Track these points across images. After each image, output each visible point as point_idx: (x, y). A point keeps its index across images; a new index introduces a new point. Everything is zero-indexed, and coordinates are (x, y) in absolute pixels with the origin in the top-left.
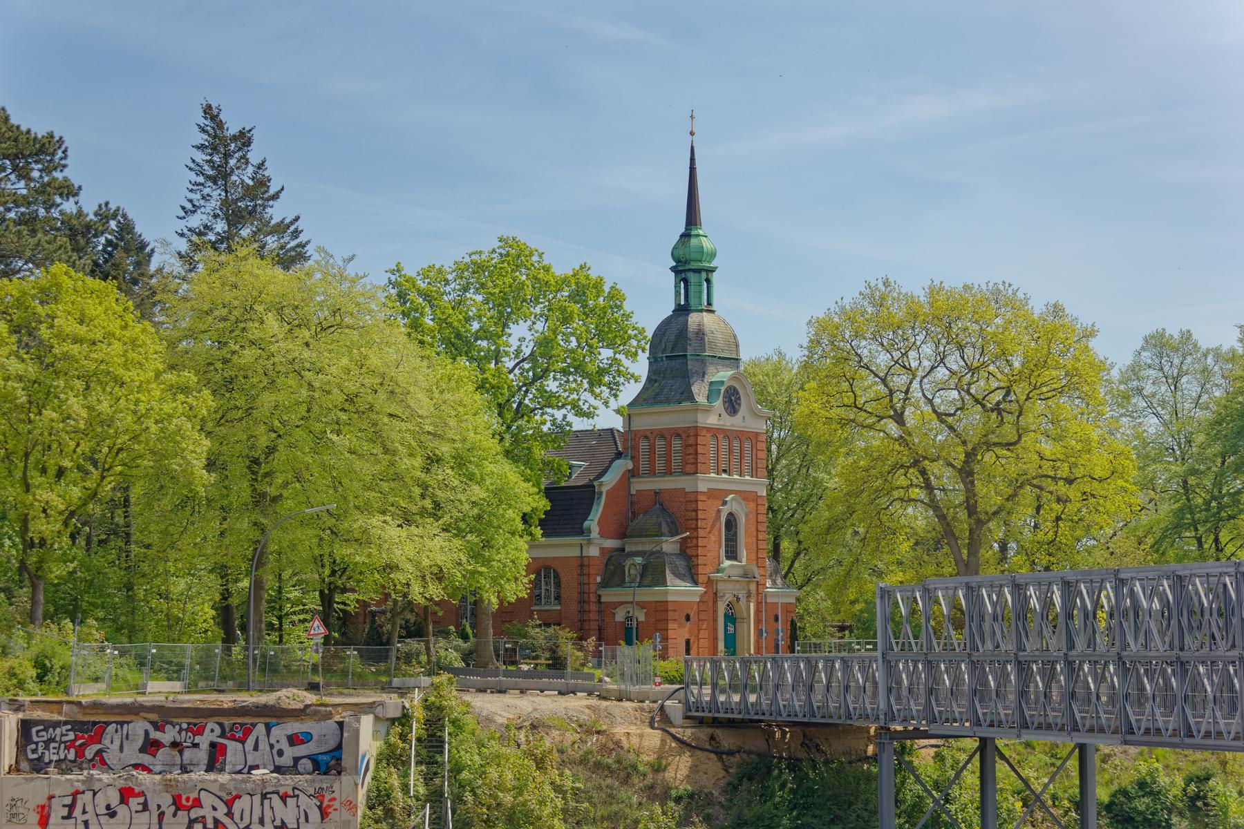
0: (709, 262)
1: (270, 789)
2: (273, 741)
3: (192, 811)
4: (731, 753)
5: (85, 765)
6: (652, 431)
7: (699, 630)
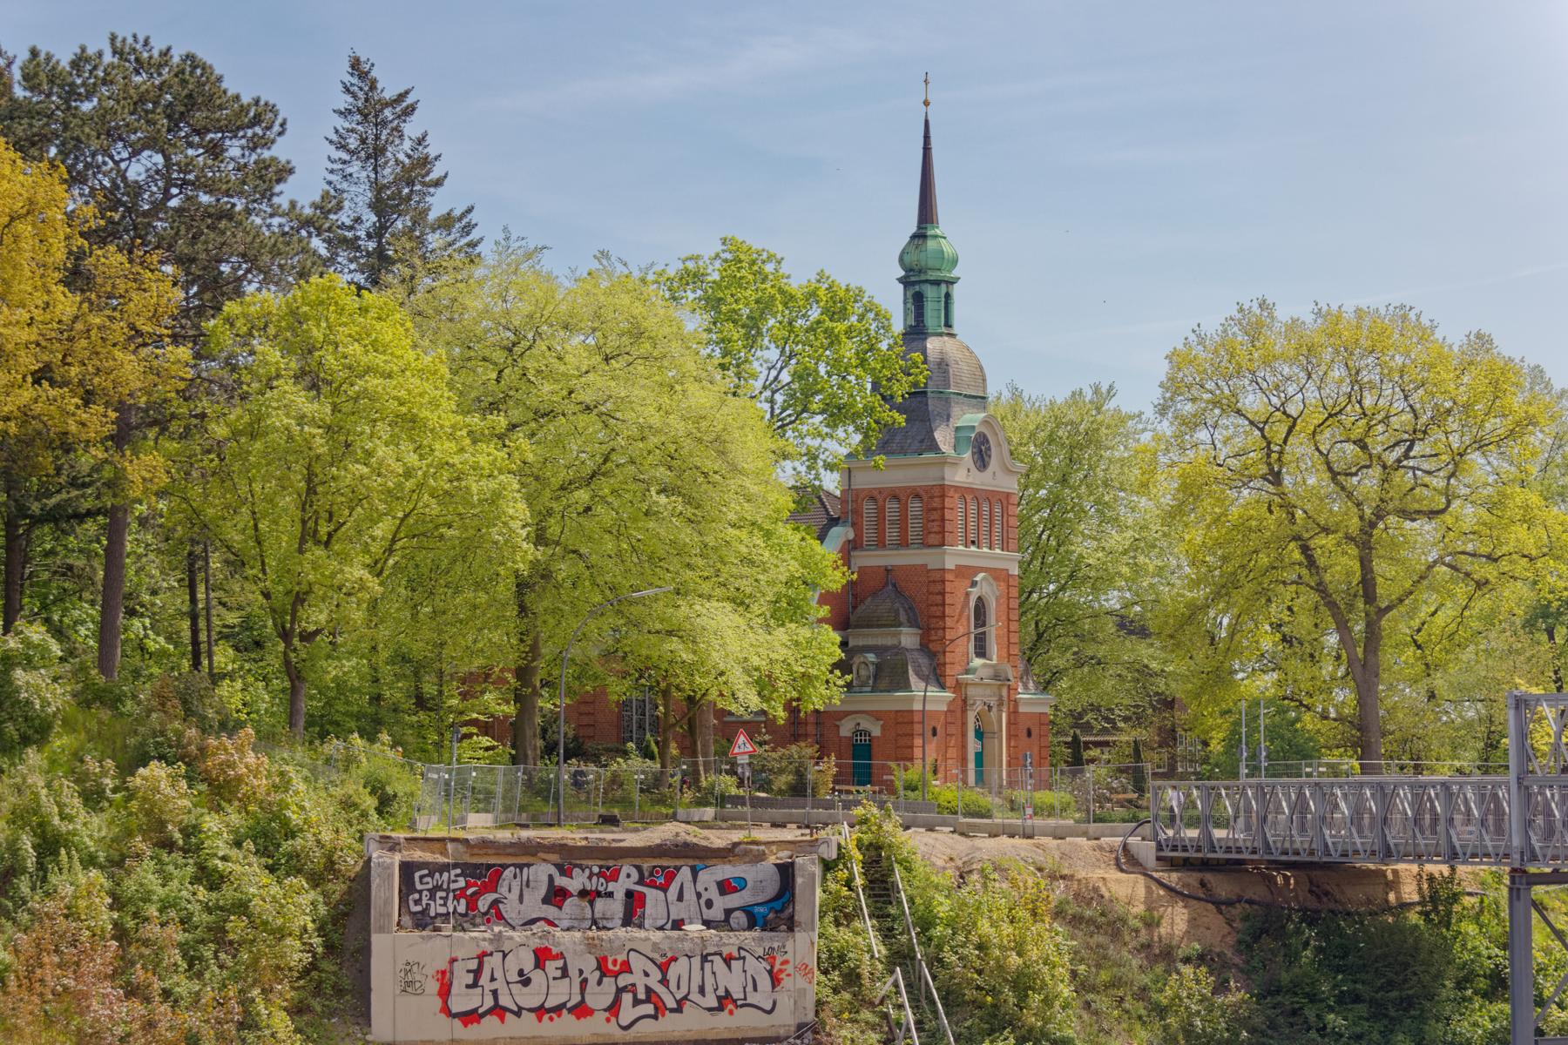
1: (711, 950)
2: (700, 888)
3: (621, 978)
5: (478, 920)
6: (880, 491)
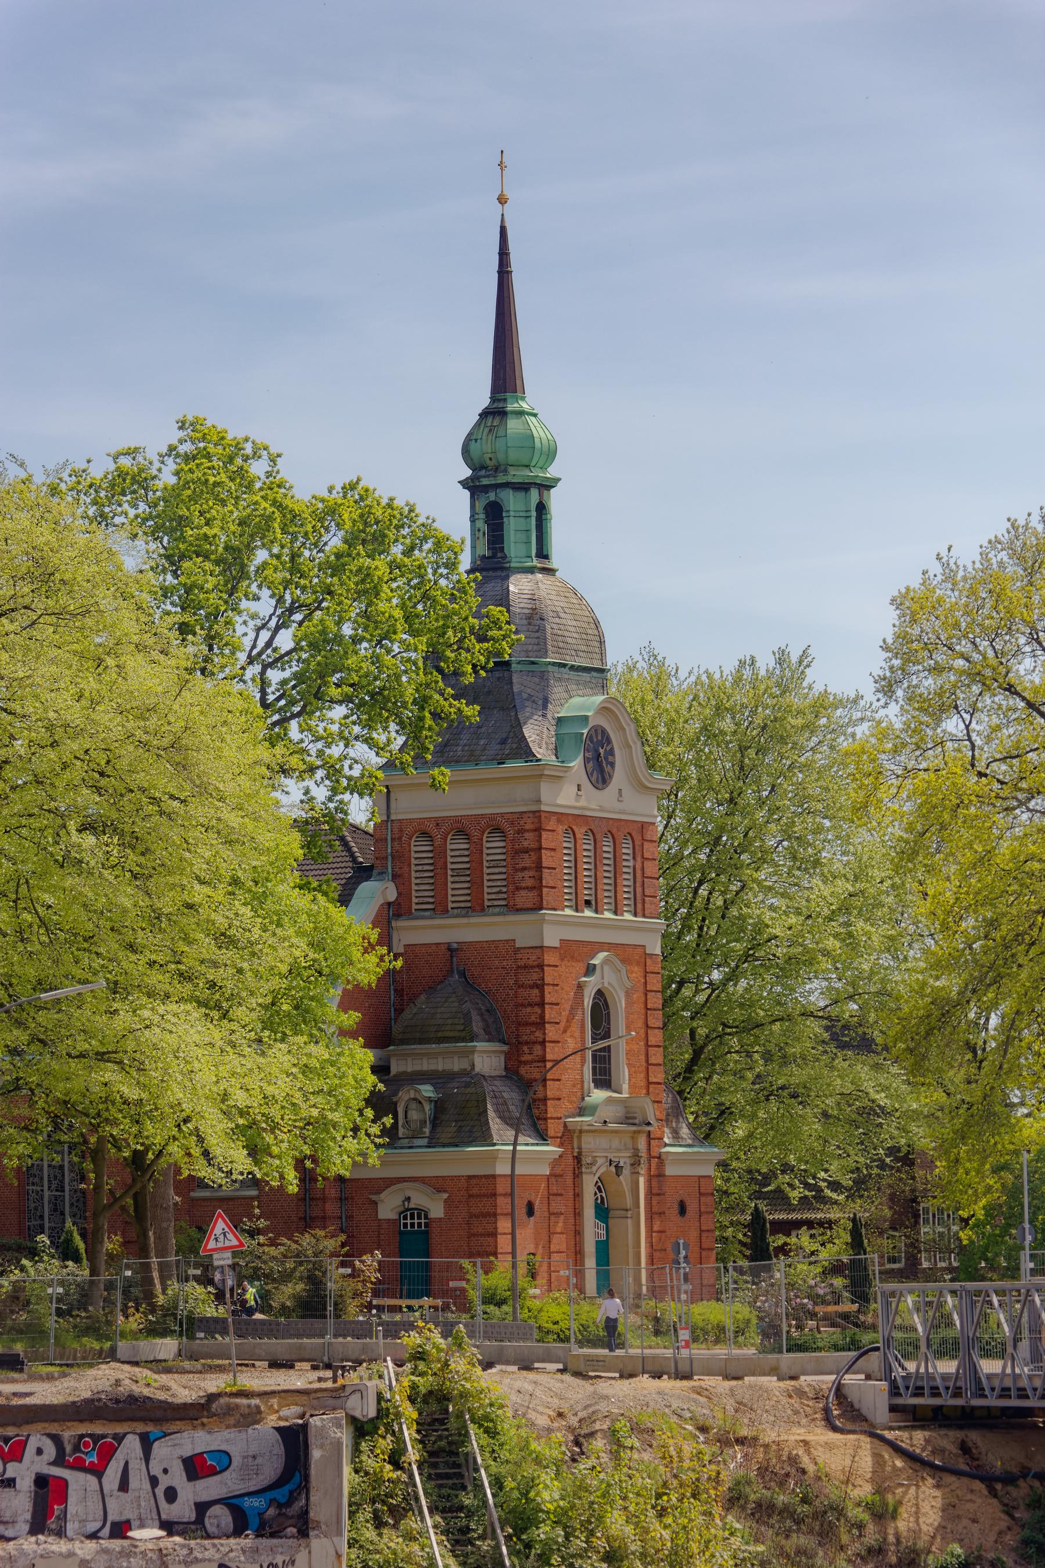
0: (544, 468)
2: (156, 1470)
4: (1009, 1479)
6: (438, 822)
7: (550, 1234)
